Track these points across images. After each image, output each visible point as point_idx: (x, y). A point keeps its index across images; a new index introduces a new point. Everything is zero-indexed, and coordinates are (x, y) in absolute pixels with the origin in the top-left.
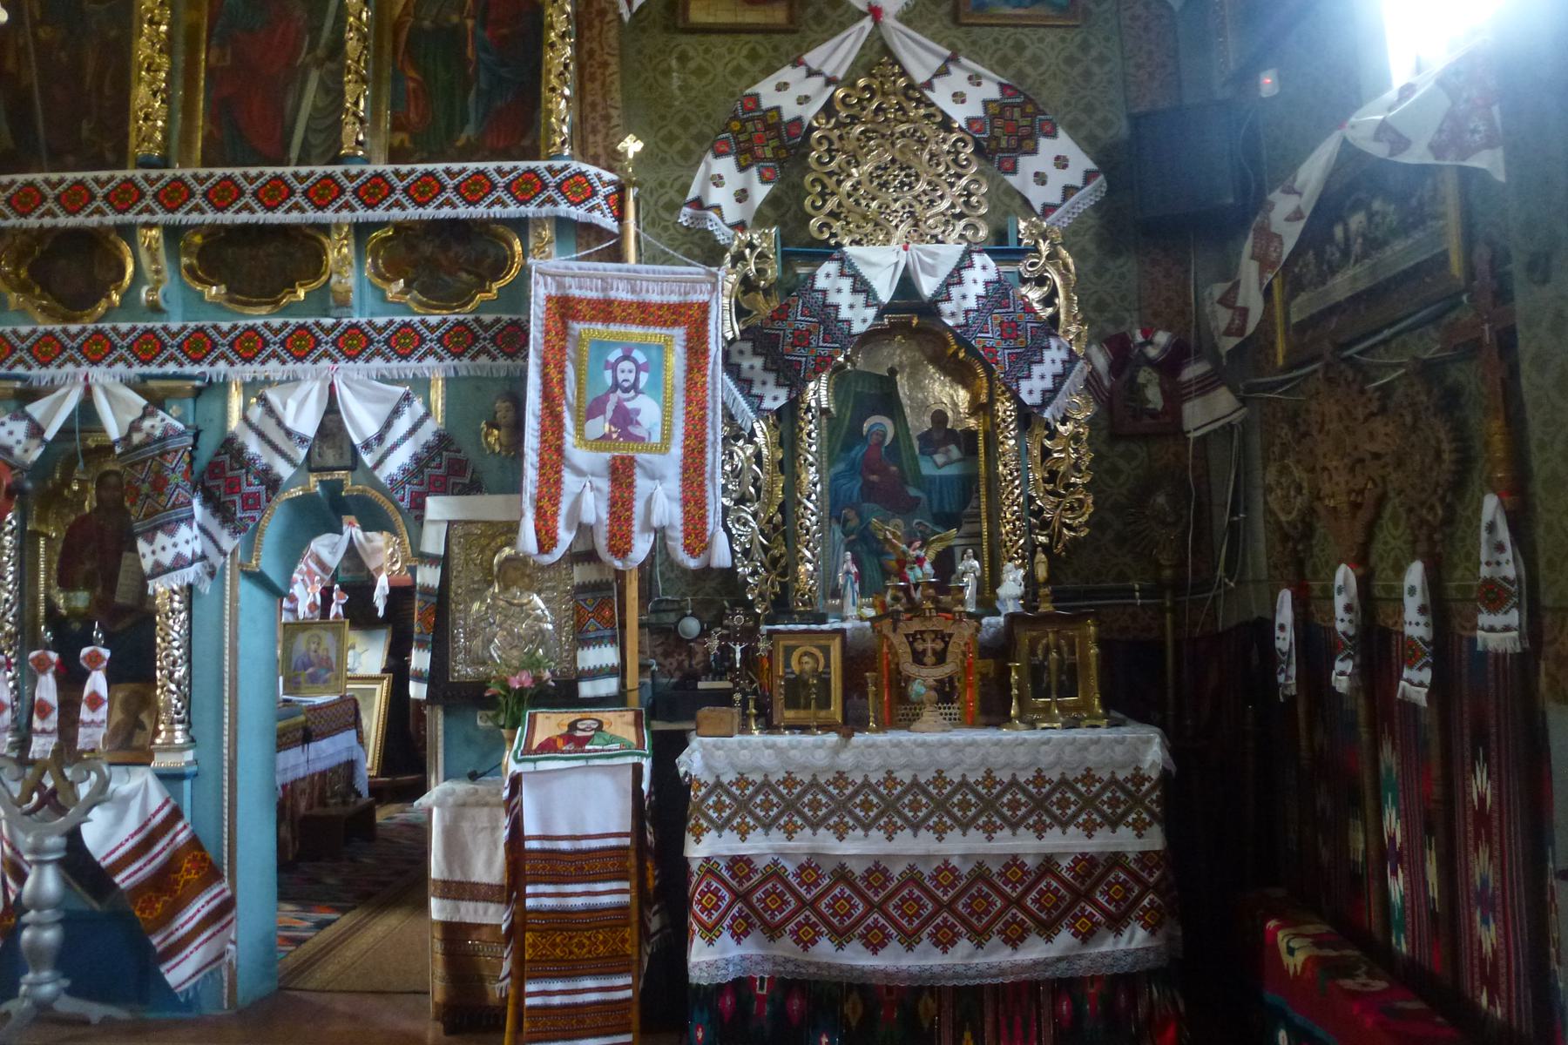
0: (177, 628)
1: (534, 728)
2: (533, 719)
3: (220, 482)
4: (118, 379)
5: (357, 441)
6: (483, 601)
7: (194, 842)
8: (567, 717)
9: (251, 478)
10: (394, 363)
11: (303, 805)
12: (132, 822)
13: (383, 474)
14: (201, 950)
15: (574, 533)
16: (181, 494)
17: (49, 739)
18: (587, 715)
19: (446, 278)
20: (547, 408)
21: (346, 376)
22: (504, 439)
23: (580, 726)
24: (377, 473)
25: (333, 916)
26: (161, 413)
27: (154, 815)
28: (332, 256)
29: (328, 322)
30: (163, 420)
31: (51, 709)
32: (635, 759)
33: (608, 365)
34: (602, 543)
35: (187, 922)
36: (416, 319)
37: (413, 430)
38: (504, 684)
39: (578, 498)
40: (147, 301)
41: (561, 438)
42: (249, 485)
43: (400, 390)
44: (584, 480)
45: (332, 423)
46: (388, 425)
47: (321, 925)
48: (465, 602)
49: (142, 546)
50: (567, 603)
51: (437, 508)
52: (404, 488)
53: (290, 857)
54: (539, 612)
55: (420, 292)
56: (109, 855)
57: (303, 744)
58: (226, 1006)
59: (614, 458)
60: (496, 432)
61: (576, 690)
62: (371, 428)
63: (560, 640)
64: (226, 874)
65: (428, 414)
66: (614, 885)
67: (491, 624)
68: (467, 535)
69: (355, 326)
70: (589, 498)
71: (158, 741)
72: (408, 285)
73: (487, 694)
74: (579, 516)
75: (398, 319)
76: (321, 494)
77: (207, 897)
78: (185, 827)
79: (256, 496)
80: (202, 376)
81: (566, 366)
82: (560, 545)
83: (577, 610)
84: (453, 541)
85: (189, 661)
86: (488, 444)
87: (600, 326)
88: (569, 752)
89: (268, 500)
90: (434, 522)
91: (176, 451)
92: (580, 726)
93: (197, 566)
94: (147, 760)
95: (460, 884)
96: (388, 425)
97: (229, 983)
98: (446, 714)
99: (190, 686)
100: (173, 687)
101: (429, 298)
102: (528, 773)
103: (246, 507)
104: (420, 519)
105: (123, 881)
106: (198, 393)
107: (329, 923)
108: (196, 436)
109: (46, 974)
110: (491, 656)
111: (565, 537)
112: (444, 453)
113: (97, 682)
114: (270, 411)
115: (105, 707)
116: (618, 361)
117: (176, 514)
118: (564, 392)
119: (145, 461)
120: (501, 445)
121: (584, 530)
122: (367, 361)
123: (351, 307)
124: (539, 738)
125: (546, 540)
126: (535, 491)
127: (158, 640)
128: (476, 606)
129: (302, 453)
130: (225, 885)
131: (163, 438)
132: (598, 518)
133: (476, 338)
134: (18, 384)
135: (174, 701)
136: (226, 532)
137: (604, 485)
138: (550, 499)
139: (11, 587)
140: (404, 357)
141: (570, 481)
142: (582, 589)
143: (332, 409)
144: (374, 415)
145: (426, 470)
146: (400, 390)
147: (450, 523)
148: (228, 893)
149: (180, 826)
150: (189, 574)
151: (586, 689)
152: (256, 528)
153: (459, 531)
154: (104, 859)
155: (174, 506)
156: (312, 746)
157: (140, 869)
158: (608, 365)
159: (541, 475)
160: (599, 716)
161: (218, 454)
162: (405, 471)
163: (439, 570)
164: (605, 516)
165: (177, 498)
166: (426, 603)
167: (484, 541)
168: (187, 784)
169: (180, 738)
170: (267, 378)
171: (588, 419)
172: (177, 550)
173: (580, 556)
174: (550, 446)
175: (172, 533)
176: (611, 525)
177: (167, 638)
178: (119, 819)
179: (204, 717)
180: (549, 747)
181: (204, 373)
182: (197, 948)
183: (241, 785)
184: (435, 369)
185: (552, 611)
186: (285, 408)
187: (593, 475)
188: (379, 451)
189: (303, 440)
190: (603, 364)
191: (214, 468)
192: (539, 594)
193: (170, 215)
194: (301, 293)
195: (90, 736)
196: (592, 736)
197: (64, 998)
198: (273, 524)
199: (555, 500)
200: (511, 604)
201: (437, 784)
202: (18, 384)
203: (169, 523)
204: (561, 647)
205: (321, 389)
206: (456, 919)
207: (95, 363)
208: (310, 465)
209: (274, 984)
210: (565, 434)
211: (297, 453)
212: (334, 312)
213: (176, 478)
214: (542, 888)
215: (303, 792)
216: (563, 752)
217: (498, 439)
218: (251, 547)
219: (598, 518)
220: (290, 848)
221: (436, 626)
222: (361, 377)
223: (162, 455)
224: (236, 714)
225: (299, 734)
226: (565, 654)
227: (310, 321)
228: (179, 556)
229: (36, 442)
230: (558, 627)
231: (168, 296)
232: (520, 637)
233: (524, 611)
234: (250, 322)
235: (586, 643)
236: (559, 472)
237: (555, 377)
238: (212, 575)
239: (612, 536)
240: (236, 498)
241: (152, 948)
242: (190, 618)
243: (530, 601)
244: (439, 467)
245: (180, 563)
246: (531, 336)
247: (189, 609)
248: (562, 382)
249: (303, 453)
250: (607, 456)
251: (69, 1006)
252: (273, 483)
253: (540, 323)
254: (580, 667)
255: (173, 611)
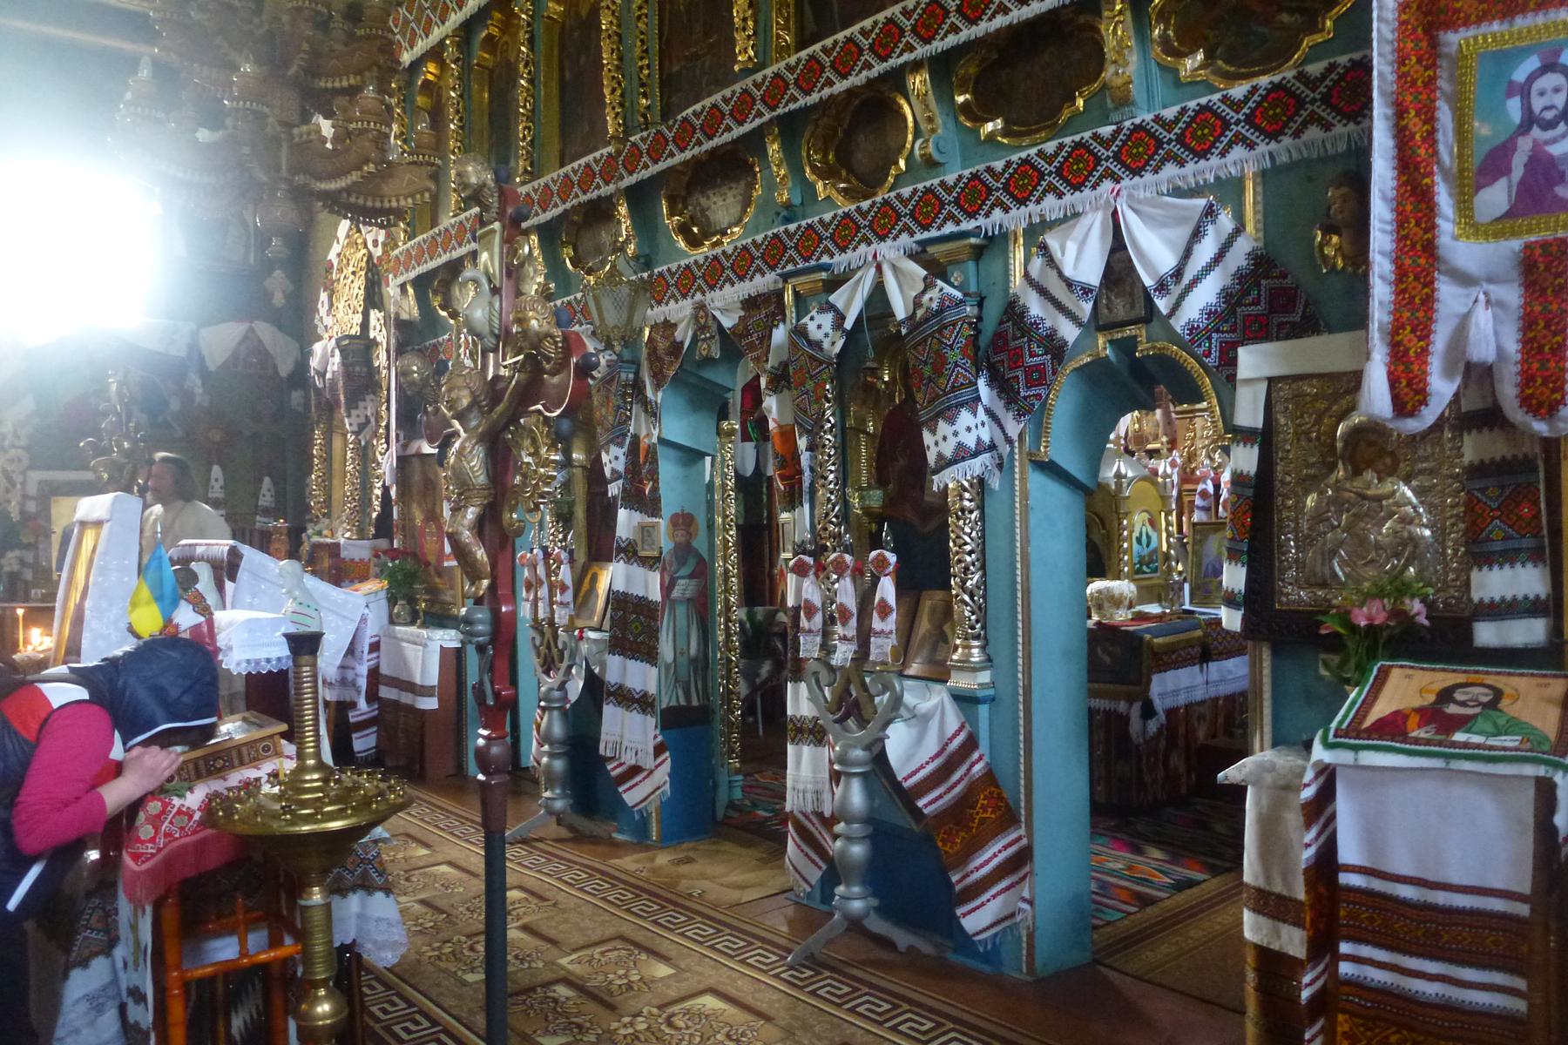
1: (1376, 698)
2: (1383, 675)
3: (1003, 356)
5: (1148, 282)
7: (989, 776)
9: (1034, 347)
10: (1191, 167)
11: (1201, 733)
12: (931, 745)
13: (1179, 324)
14: (1000, 898)
15: (1458, 381)
16: (962, 374)
18: (1473, 678)
19: (1261, 29)
20: (1405, 184)
21: (1130, 196)
22: (1346, 247)
24: (1172, 321)
25: (1199, 876)
26: (939, 283)
27: (951, 739)
28: (1110, 44)
29: (1106, 131)
30: (941, 290)
31: (892, 610)
32: (1541, 771)
34: (1508, 392)
35: (982, 866)
36: (1216, 97)
37: (1218, 258)
38: (1345, 617)
39: (1464, 320)
41: (1432, 227)
42: (1032, 356)
43: (1201, 203)
44: (1475, 292)
45: (1119, 268)
46: (1187, 254)
47: (1182, 885)
48: (1296, 495)
49: (928, 438)
50: (1455, 494)
51: (1253, 361)
52: (1210, 338)
53: (1183, 790)
54: (1409, 509)
55: (1226, 61)
57: (1201, 663)
58: (1024, 970)
59: (1528, 247)
60: (1335, 239)
61: (1469, 635)
63: (1444, 554)
64: (1023, 819)
65: (1239, 230)
66: (1498, 978)
67: (1334, 528)
68: (1297, 397)
69: (1139, 128)
70: (1483, 319)
71: (955, 657)
74: (1464, 353)
75: (1192, 104)
76: (1113, 358)
78: (980, 758)
79: (1040, 369)
80: (976, 232)
81: (1439, 114)
82: (1433, 401)
83: (1470, 506)
84: (1279, 407)
85: (983, 567)
86: (1325, 258)
87: (1496, 26)
88: (1428, 742)
89: (1054, 373)
90: (1248, 381)
93: (985, 458)
94: (943, 677)
95: (1280, 897)
96: (1187, 254)
97: (1028, 943)
98: (1276, 653)
99: (984, 597)
100: (966, 598)
102: (1346, 766)
103: (1030, 384)
105: (926, 806)
106: (978, 253)
107: (1191, 884)
108: (980, 305)
109: (856, 889)
110: (1335, 575)
111: (1442, 388)
112: (1263, 282)
113: (887, 589)
114: (1051, 262)
116: (1532, 78)
117: (956, 397)
118: (1436, 153)
119: (925, 340)
120: (1344, 258)
121: (1478, 375)
123: (1133, 103)
124: (1381, 709)
125: (1408, 394)
126: (1387, 319)
127: (951, 544)
128: (1310, 501)
130: (1022, 831)
132: (1500, 351)
133: (1300, 103)
134: (824, 275)
135: (967, 614)
137: (1512, 295)
139: (832, 486)
140: (1202, 154)
141: (1449, 297)
142: (1478, 471)
143: (1118, 246)
144: (1170, 243)
146: (1201, 203)
148: (1024, 841)
149: (976, 756)
150: (976, 465)
151: (1486, 634)
152: (1044, 404)
153: (1285, 391)
154: (906, 779)
155: (954, 389)
156: (1213, 666)
157: (940, 797)
158: (1511, 89)
160: (1500, 682)
161: (1001, 323)
162: (1210, 313)
163: (1256, 450)
164: (1512, 346)
165: (956, 379)
166: (1239, 497)
167: (1322, 405)
168: (983, 710)
169: (976, 655)
170: (1043, 221)
171: (1479, 188)
173: (1464, 419)
174: (1413, 246)
175: (951, 421)
176: (1523, 362)
179: (998, 633)
180: (1392, 729)
181: (979, 227)
182: (994, 897)
184: (1243, 162)
185: (1431, 508)
186: (1063, 254)
187: (1490, 280)
188: (1176, 290)
190: (1504, 86)
191: (999, 338)
192: (1407, 480)
193: (928, 47)
194: (1080, 103)
196: (1474, 717)
197: (873, 917)
198: (1064, 401)
199: (1423, 331)
200: (1364, 497)
201: (1262, 749)
202: (824, 275)
203: (949, 408)
204: (1446, 564)
205: (1103, 224)
206: (1275, 946)
207: (882, 238)
208: (1098, 323)
209: (1087, 957)
210: (1439, 221)
211: (1082, 310)
212: (1115, 117)
213: (954, 356)
214: (1366, 951)
215: (1201, 717)
216: (1417, 741)
217: (1339, 249)
219: (1500, 351)
220: (1184, 780)
222: (1148, 194)
223: (940, 331)
225: (1197, 650)
226: (1451, 576)
228: (960, 446)
229: (839, 333)
230: (1440, 533)
232: (1378, 546)
233: (1377, 507)
234: (1023, 155)
235: (1485, 558)
236: (1429, 284)
238: (1000, 466)
239: (1527, 379)
240: (1020, 373)
241: (950, 886)
242: (982, 518)
243: (1394, 492)
244: (1256, 303)
245: (962, 454)
246: (1375, 73)
247: (981, 507)
248: (1430, 138)
249: (1087, 307)
250: (1516, 244)
251: (878, 925)
252: (1056, 349)
253: (1388, 48)
254: (1476, 596)
255: (963, 510)
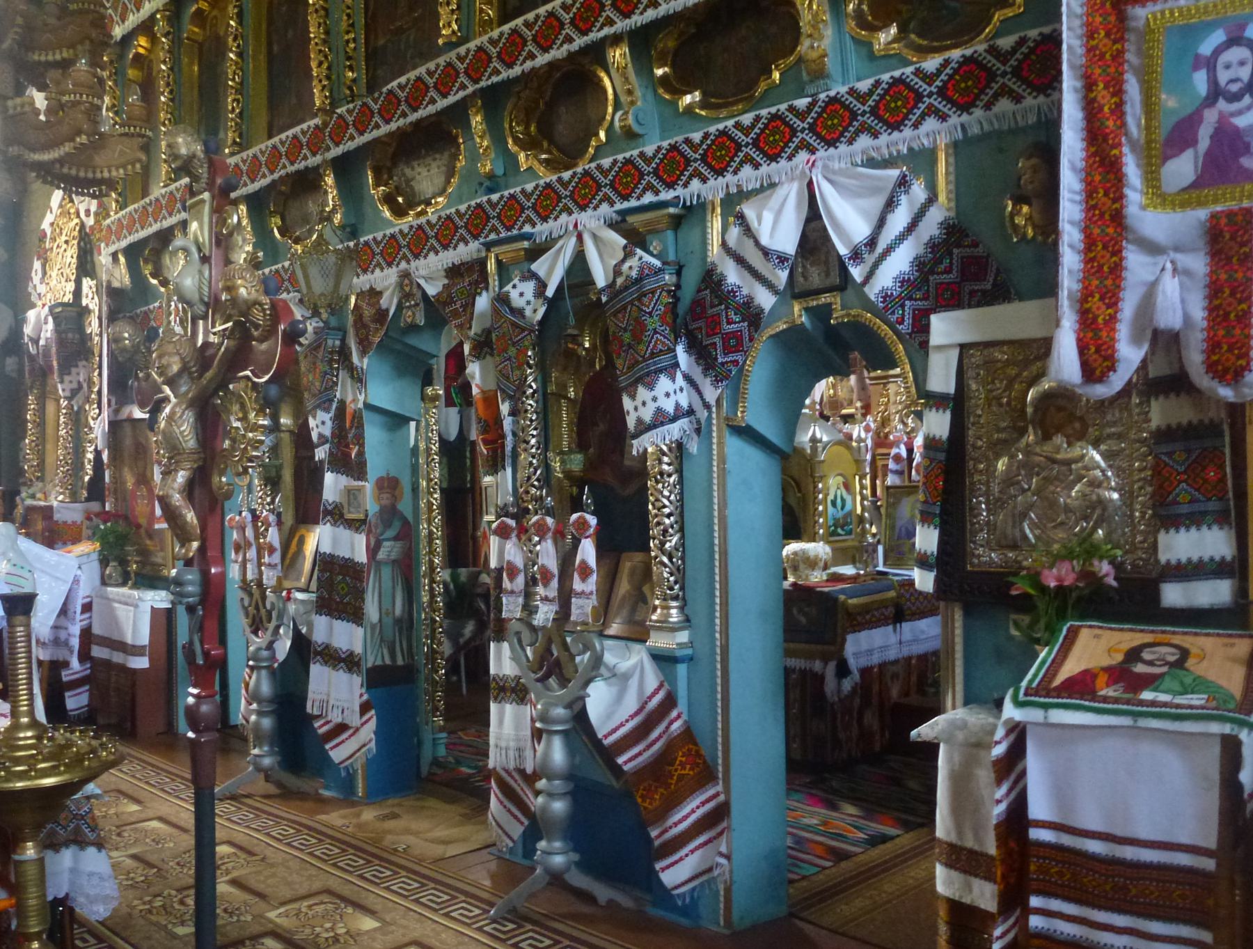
0: (666, 493)
1: (1065, 657)
3: (701, 323)
4: (602, 221)
5: (843, 250)
6: (1012, 457)
7: (688, 734)
8: (1127, 638)
11: (895, 692)
12: (631, 703)
13: (873, 291)
15: (1146, 347)
16: (661, 340)
17: (551, 607)
20: (1094, 155)
21: (825, 167)
22: (1036, 216)
23: (1146, 655)
24: (866, 289)
25: (892, 831)
27: (650, 698)
30: (640, 258)
31: (592, 572)
32: (1227, 729)
33: (1198, 62)
34: (1195, 358)
35: (680, 821)
36: (909, 70)
39: (1151, 291)
40: (621, 127)
41: (1120, 197)
42: (729, 322)
43: (894, 173)
46: (881, 223)
47: (876, 840)
48: (987, 459)
49: (627, 403)
52: (903, 306)
54: (1098, 473)
55: (919, 35)
56: (610, 733)
57: (895, 623)
59: (1213, 216)
60: (1025, 209)
61: (1156, 596)
62: (860, 229)
63: (1132, 516)
64: (720, 775)
65: (932, 200)
68: (989, 363)
69: (834, 100)
70: (1170, 287)
71: (654, 617)
72: (903, 30)
73: (1014, 593)
74: (1151, 320)
75: (886, 77)
76: (808, 325)
77: (703, 797)
78: (679, 716)
79: (737, 335)
83: (1158, 470)
84: (970, 373)
85: (682, 530)
86: (1015, 227)
88: (1116, 701)
89: (751, 340)
90: (940, 348)
91: (653, 292)
92: (1146, 655)
93: (683, 423)
95: (971, 852)
96: (881, 223)
98: (967, 614)
99: (682, 558)
100: (665, 559)
101: (933, 40)
103: (727, 350)
104: (924, 345)
105: (626, 763)
106: (677, 222)
107: (885, 839)
108: (679, 273)
110: (1025, 537)
112: (955, 251)
113: (588, 551)
114: (748, 231)
115: (594, 578)
116: (1218, 51)
122: (850, 142)
123: (828, 76)
124: (1070, 668)
126: (1076, 287)
127: (650, 507)
128: (1001, 465)
129: (782, 276)
130: (720, 788)
131: (639, 280)
132: (1187, 318)
134: (526, 244)
135: (666, 575)
136: (708, 380)
137: (1198, 263)
138: (1102, 299)
139: (534, 450)
140: (895, 126)
141: (1137, 265)
142: (1165, 435)
143: (813, 216)
144: (864, 213)
145: (931, 278)
146: (894, 173)
147: (963, 347)
148: (722, 798)
149: (674, 714)
150: (675, 430)
151: (1173, 595)
152: (741, 370)
153: (976, 357)
154: (606, 737)
155: (653, 355)
156: (907, 627)
157: (640, 754)
158: (1198, 62)
159: (1088, 261)
161: (699, 291)
163: (948, 414)
164: (1199, 313)
165: (655, 346)
167: (1012, 371)
168: (682, 669)
169: (675, 616)
172: (656, 405)
174: (1102, 215)
175: (651, 386)
177: (657, 504)
178: (619, 698)
182: (692, 852)
183: (733, 677)
185: (1119, 472)
186: (760, 224)
187: (1177, 249)
188: (870, 259)
189: (782, 259)
190: (1190, 60)
192: (1096, 445)
193: (627, 21)
194: (776, 75)
195: (582, 607)
196: (1162, 675)
199: (1112, 298)
200: (1054, 461)
201: (954, 708)
202: (526, 244)
203: (648, 374)
204: (1134, 526)
205: (799, 194)
206: (967, 900)
207: (583, 208)
208: (794, 291)
209: (783, 910)
210: (1127, 191)
211: (778, 278)
213: (653, 323)
214: (1056, 905)
215: (895, 676)
216: (1105, 699)
217: (1029, 219)
218: (737, 395)
219: (1187, 318)
220: (877, 737)
221: (946, 491)
223: (639, 299)
224: (727, 592)
225: (891, 610)
226: (1139, 538)
227: (783, 107)
229: (541, 301)
230: (1128, 497)
231: (640, 117)
233: (1067, 471)
234: (721, 126)
235: (1173, 522)
236: (1118, 252)
237: (1106, 100)
239: (1213, 345)
240: (717, 340)
241: (650, 841)
242: (681, 481)
243: (1083, 456)
244: (948, 271)
245: (661, 419)
246: (1065, 47)
247: (680, 471)
248: (1119, 111)
250: (1202, 214)
251: (579, 880)
252: (754, 317)
253: (1077, 23)
255: (662, 474)
